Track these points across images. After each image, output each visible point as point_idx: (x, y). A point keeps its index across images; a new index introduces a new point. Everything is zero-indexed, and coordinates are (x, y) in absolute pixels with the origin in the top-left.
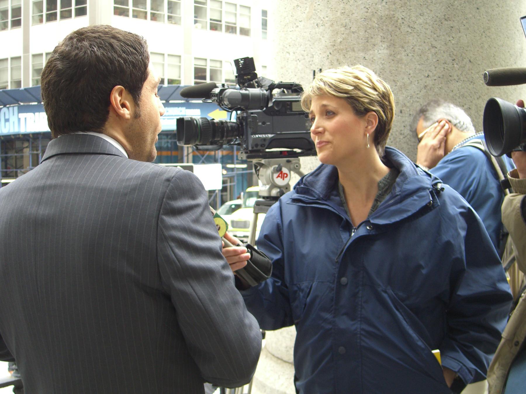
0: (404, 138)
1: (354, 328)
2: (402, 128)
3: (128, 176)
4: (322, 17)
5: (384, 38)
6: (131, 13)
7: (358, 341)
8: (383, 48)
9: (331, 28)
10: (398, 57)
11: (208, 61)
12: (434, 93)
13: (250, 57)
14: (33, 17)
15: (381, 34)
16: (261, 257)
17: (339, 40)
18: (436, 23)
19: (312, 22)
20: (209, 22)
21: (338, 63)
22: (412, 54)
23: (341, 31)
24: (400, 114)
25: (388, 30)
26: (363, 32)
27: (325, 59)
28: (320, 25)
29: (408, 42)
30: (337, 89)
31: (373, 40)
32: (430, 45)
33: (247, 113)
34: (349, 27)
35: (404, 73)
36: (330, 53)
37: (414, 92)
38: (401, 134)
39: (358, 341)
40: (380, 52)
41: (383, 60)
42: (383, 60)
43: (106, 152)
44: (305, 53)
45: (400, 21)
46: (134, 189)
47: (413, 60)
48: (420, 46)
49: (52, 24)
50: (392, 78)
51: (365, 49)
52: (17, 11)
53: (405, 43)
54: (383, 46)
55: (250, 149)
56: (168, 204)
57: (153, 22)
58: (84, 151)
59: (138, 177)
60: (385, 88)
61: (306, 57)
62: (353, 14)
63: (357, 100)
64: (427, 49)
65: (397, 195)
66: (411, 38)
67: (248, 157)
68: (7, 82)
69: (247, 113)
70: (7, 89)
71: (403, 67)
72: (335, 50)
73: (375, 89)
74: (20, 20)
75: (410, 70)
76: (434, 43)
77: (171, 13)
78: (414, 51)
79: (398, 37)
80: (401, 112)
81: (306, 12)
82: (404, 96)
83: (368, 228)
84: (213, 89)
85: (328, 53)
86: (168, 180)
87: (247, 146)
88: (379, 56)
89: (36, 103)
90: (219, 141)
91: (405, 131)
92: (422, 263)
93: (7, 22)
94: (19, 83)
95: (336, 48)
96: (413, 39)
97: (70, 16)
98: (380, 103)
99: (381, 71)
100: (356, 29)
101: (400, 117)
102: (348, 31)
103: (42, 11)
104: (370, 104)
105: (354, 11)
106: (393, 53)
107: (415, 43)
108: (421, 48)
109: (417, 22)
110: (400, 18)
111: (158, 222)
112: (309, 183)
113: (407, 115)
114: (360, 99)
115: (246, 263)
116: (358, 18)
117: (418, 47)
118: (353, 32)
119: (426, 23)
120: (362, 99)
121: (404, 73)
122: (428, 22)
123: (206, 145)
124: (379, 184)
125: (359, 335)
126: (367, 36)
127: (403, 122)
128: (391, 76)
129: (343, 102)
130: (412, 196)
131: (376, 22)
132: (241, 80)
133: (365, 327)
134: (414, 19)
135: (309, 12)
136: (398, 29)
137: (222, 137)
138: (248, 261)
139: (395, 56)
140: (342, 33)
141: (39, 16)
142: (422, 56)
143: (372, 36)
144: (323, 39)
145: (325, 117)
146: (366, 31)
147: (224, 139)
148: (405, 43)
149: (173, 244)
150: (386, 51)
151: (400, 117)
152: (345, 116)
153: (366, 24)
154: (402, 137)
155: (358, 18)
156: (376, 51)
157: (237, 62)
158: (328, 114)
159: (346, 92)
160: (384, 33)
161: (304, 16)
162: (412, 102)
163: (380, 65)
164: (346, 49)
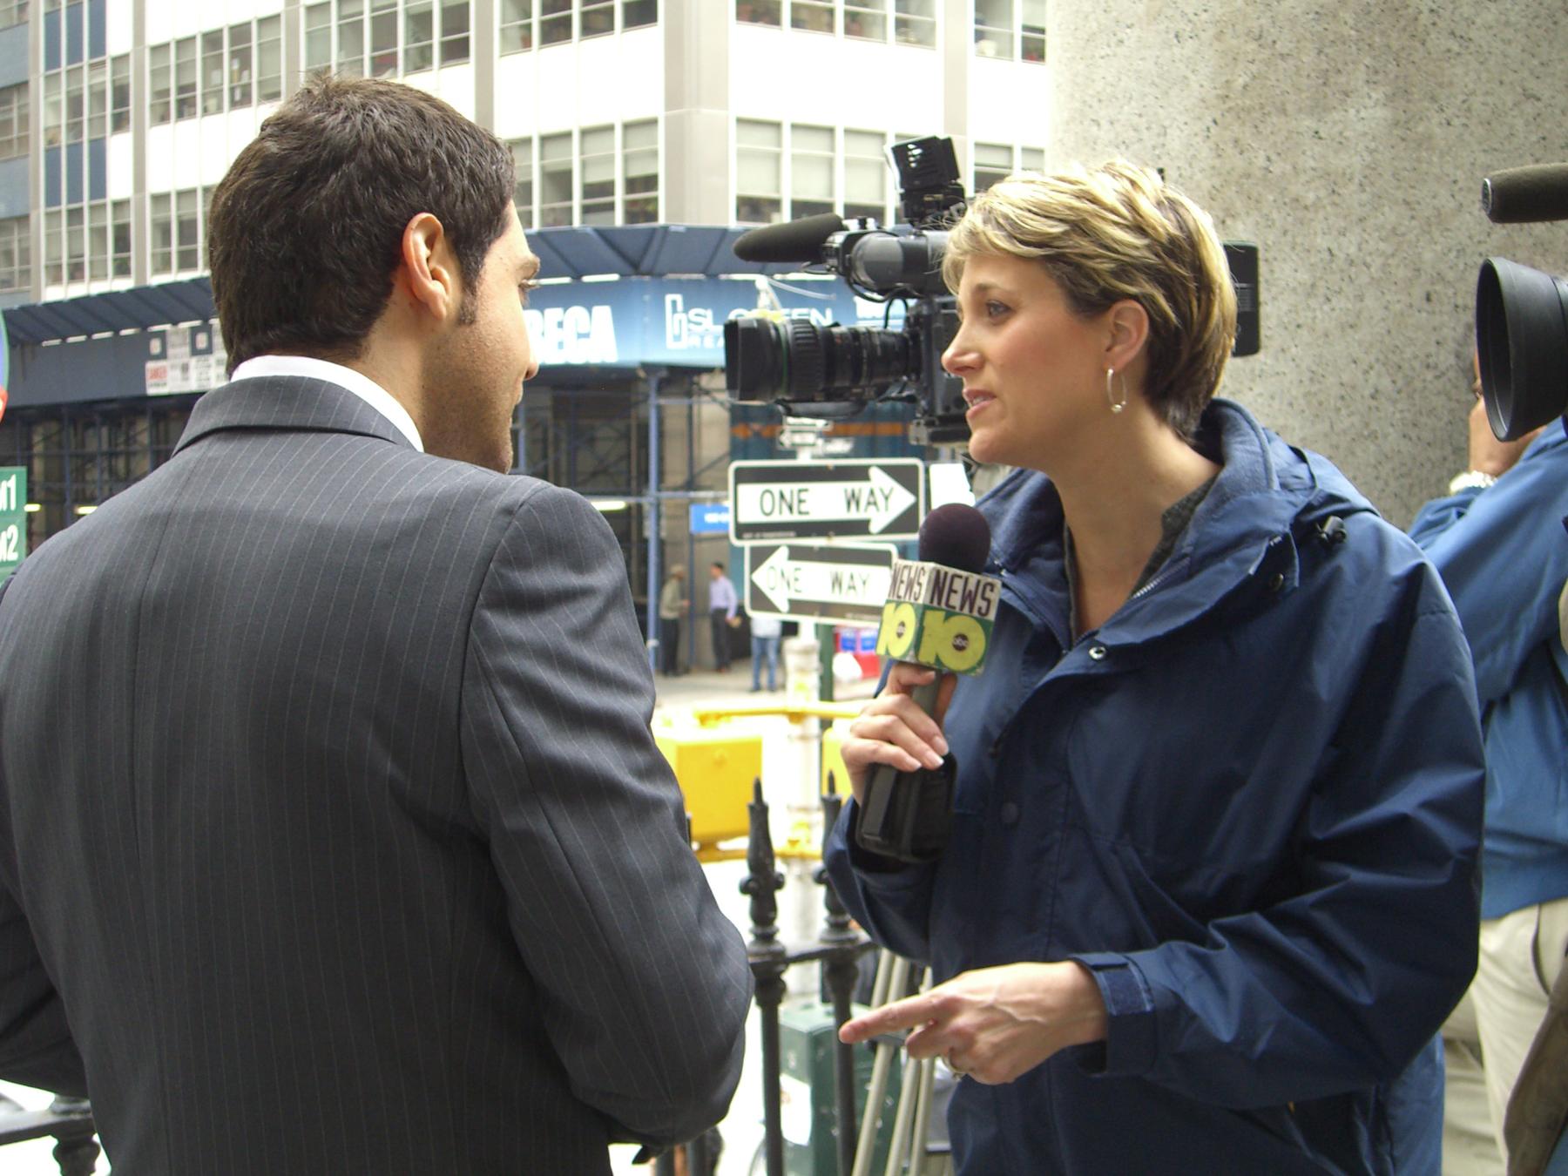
0: (1437, 377)
2: (1433, 349)
3: (399, 493)
4: (1190, 11)
5: (1376, 72)
8: (1371, 103)
9: (1217, 45)
10: (1421, 129)
11: (1017, 153)
12: (1531, 241)
13: (942, 136)
14: (503, 30)
15: (1368, 61)
17: (1241, 81)
18: (1538, 22)
19: (1162, 27)
20: (1018, 34)
21: (1236, 151)
22: (1464, 121)
23: (1246, 53)
24: (1426, 306)
25: (1389, 47)
26: (1313, 54)
27: (1198, 139)
28: (1187, 34)
29: (1451, 84)
30: (1015, 232)
31: (1342, 79)
32: (1519, 90)
33: (930, 303)
34: (1270, 40)
35: (1438, 179)
36: (1215, 122)
37: (1470, 237)
38: (1428, 366)
40: (1363, 114)
41: (1374, 139)
42: (1374, 139)
43: (350, 428)
44: (1143, 123)
45: (1425, 18)
46: (408, 533)
47: (1467, 137)
48: (1487, 93)
49: (558, 50)
50: (1400, 195)
51: (1318, 108)
52: (456, 18)
53: (1441, 85)
54: (1374, 95)
55: (940, 411)
56: (501, 576)
57: (855, 43)
58: (290, 420)
59: (424, 500)
60: (1182, 224)
61: (1145, 135)
63: (1079, 267)
64: (1510, 104)
65: (1185, 556)
66: (1459, 71)
67: (935, 438)
69: (930, 303)
71: (1435, 159)
73: (1139, 228)
75: (1457, 168)
76: (1532, 85)
77: (906, 12)
78: (1469, 110)
79: (1418, 69)
80: (1428, 299)
82: (1438, 248)
84: (830, 233)
85: (1208, 121)
86: (508, 511)
87: (931, 404)
88: (1360, 127)
89: (566, 280)
90: (849, 388)
91: (1442, 358)
93: (430, 47)
95: (1232, 104)
96: (1466, 74)
98: (1159, 271)
99: (1368, 172)
100: (1291, 46)
101: (1424, 314)
102: (1266, 54)
103: (528, 15)
104: (1116, 274)
106: (1403, 117)
107: (1471, 86)
108: (1490, 100)
109: (1479, 21)
110: (1426, 11)
111: (468, 633)
113: (1448, 308)
114: (1084, 261)
116: (1298, 11)
117: (1481, 99)
118: (1283, 56)
119: (1507, 24)
120: (1090, 263)
121: (1438, 179)
122: (1513, 19)
123: (813, 400)
124: (1164, 517)
126: (1325, 66)
127: (1435, 329)
128: (1398, 188)
129: (1036, 272)
130: (1222, 561)
131: (1351, 22)
132: (916, 208)
134: (1467, 11)
136: (1418, 45)
137: (856, 377)
139: (1411, 125)
140: (1250, 58)
141: (522, 27)
142: (1494, 124)
143: (1340, 66)
144: (1192, 77)
145: (987, 319)
146: (1320, 52)
147: (863, 382)
148: (1441, 85)
149: (506, 693)
150: (1381, 113)
151: (1424, 314)
152: (1041, 314)
153: (1320, 28)
154: (1429, 376)
155: (1298, 11)
156: (1352, 112)
157: (900, 152)
158: (995, 310)
159: (1043, 242)
160: (1374, 58)
162: (1461, 266)
163: (1365, 154)
164: (1262, 107)
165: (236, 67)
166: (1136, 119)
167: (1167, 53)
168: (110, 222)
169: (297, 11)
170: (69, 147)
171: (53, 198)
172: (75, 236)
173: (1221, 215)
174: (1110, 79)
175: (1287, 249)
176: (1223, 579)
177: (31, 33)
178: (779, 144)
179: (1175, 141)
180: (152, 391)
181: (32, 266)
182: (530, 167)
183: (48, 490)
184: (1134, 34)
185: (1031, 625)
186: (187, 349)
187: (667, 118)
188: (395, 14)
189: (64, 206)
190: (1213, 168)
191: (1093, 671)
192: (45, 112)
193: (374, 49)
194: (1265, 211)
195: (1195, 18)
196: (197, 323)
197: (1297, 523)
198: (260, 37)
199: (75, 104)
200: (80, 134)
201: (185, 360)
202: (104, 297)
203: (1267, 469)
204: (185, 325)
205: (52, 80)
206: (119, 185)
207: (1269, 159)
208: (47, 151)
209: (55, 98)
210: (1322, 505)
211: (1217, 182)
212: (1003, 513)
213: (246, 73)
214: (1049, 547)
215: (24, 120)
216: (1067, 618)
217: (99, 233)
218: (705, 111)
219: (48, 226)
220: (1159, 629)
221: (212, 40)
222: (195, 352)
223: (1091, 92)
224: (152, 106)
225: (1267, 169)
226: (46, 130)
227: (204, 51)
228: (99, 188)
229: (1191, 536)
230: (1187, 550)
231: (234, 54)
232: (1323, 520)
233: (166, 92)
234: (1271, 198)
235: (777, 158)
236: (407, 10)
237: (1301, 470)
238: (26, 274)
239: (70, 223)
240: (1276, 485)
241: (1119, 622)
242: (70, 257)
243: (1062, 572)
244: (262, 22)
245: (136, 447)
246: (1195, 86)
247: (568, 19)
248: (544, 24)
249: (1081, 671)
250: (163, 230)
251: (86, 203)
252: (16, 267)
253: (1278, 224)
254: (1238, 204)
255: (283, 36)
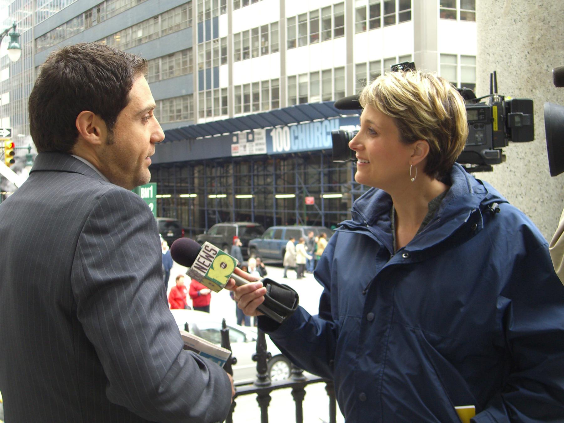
1: (375, 371)
6: (458, 15)
7: (379, 387)
9: (529, 24)
14: (356, 25)
16: (283, 289)
17: (537, 37)
19: (510, 17)
21: (536, 64)
27: (523, 59)
28: (518, 20)
36: (528, 53)
39: (379, 387)
44: (503, 54)
49: (376, 31)
52: (340, 20)
61: (504, 58)
62: (552, 6)
65: (438, 218)
68: (331, 94)
70: (330, 101)
72: (534, 48)
74: (343, 29)
81: (504, 7)
83: (404, 256)
85: (526, 53)
92: (462, 298)
93: (330, 31)
94: (343, 94)
97: (394, 22)
102: (547, 26)
103: (365, 19)
105: (552, 3)
112: (358, 207)
115: (263, 298)
125: (380, 381)
130: (453, 219)
133: (389, 371)
135: (506, 7)
138: (265, 296)
140: (540, 28)
155: (558, 10)
161: (502, 11)
164: (545, 47)
165: (263, 40)
166: (501, 52)
167: (512, 27)
168: (220, 96)
169: (284, 21)
170: (207, 70)
171: (201, 88)
172: (208, 101)
173: (531, 88)
174: (493, 38)
175: (555, 100)
176: (454, 226)
177: (193, 31)
178: (456, 62)
179: (515, 61)
180: (234, 154)
181: (194, 111)
182: (366, 73)
183: (200, 190)
184: (499, 21)
185: (379, 245)
186: (245, 140)
187: (415, 55)
188: (318, 20)
189: (205, 90)
190: (528, 70)
191: (404, 262)
192: (198, 58)
193: (311, 33)
194: (547, 86)
195: (521, 14)
196: (249, 131)
197: (481, 206)
198: (271, 30)
199: (208, 55)
200: (210, 65)
201: (244, 144)
202: (218, 122)
203: (469, 186)
204: (245, 132)
205: (200, 46)
206: (223, 83)
207: (548, 66)
208: (199, 71)
209: (201, 53)
210: (490, 199)
211: (529, 75)
212: (368, 204)
213: (266, 43)
214: (385, 216)
215: (191, 60)
216: (393, 243)
217: (217, 100)
218: (428, 51)
219: (200, 97)
220: (429, 245)
221: (255, 31)
222: (248, 141)
223: (487, 43)
224: (235, 55)
225: (547, 70)
226: (199, 64)
227: (252, 35)
228: (217, 84)
229: (441, 210)
230: (439, 216)
231: (262, 36)
232: (491, 204)
233: (239, 50)
234: (549, 81)
235: (455, 68)
236: (322, 19)
237: (481, 187)
238: (192, 114)
239: (207, 96)
240: (472, 191)
241: (412, 243)
242: (207, 108)
243: (391, 226)
244: (272, 24)
245: (229, 175)
246: (521, 39)
247: (379, 20)
248: (371, 22)
249: (400, 263)
250: (238, 98)
251: (212, 89)
252: (189, 112)
253: (551, 91)
254: (537, 84)
255: (279, 29)
